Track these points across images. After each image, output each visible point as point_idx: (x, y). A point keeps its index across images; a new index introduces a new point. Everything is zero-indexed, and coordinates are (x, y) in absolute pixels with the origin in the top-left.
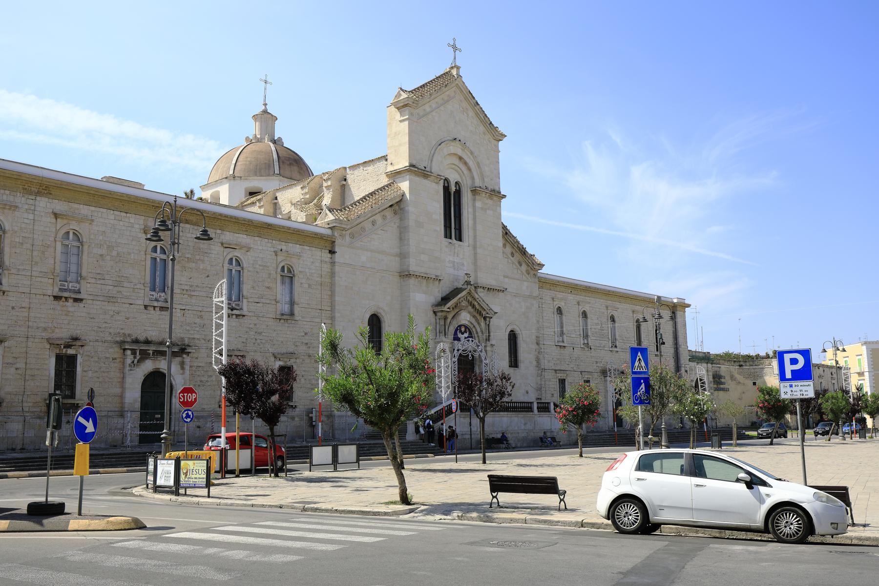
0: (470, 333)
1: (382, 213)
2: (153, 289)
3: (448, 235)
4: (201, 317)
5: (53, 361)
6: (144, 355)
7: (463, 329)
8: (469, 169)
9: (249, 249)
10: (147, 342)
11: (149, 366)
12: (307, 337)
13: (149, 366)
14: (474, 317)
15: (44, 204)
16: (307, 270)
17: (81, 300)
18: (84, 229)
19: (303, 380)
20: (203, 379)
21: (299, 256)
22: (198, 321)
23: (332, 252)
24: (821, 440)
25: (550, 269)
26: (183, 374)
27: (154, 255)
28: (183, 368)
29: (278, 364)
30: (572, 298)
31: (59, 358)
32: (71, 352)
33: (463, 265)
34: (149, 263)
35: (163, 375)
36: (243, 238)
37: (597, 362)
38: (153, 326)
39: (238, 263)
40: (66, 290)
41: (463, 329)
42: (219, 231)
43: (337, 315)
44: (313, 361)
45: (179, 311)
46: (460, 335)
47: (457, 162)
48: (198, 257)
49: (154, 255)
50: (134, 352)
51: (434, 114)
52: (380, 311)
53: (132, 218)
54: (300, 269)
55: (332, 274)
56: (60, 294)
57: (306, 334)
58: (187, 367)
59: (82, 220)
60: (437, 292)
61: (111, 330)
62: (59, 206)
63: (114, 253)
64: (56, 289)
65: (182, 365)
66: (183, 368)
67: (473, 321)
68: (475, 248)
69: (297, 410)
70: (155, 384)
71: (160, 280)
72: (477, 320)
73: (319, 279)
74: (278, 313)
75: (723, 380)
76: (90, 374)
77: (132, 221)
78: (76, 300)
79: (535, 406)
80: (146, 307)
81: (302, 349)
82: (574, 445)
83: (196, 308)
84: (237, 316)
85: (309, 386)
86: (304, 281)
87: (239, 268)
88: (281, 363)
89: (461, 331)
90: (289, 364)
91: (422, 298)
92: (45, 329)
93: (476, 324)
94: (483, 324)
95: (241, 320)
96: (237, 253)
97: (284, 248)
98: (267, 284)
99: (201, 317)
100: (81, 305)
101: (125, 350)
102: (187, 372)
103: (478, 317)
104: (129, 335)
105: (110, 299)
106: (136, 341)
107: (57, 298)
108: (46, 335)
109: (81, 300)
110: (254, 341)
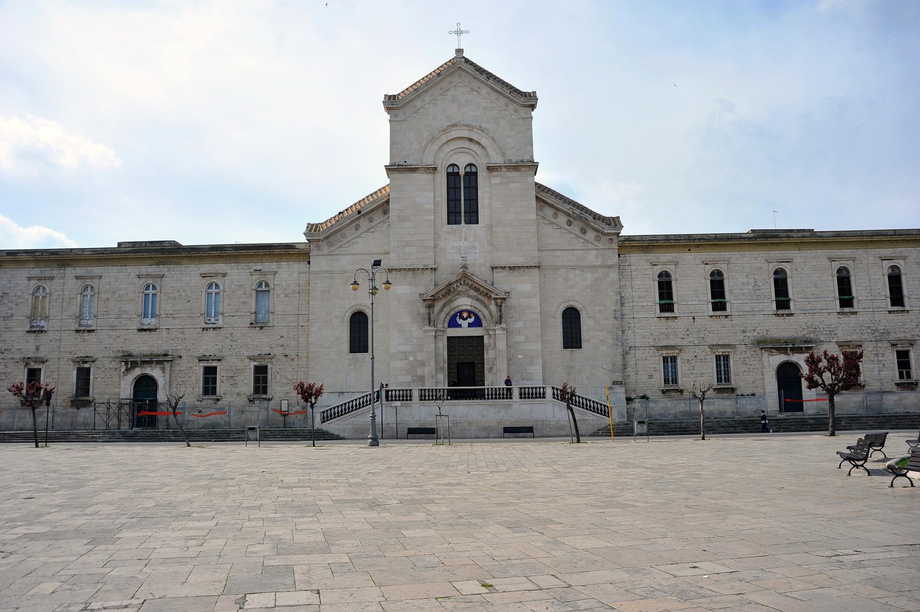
0: (455, 316)
1: (368, 217)
3: (453, 217)
4: (183, 333)
5: (75, 372)
6: (135, 364)
7: (465, 315)
9: (224, 275)
11: (137, 372)
13: (137, 372)
14: (478, 300)
15: (70, 272)
16: (284, 282)
17: (93, 331)
19: (278, 377)
23: (309, 263)
24: (725, 412)
29: (253, 364)
30: (863, 254)
31: (79, 370)
32: (86, 366)
33: (475, 247)
36: (220, 267)
37: (744, 332)
38: (142, 345)
39: (154, 287)
41: (465, 315)
46: (460, 321)
50: (126, 363)
56: (206, 326)
59: (92, 278)
60: (426, 285)
62: (80, 271)
63: (117, 295)
64: (28, 326)
67: (478, 305)
70: (145, 386)
72: (482, 303)
76: (99, 380)
82: (697, 432)
83: (178, 327)
84: (214, 329)
85: (285, 381)
86: (280, 292)
88: (256, 363)
90: (264, 363)
91: (406, 291)
92: (70, 353)
93: (481, 307)
95: (218, 331)
96: (214, 280)
98: (242, 300)
99: (183, 333)
100: (93, 334)
103: (486, 300)
105: (113, 328)
107: (77, 331)
108: (70, 356)
109: (93, 331)
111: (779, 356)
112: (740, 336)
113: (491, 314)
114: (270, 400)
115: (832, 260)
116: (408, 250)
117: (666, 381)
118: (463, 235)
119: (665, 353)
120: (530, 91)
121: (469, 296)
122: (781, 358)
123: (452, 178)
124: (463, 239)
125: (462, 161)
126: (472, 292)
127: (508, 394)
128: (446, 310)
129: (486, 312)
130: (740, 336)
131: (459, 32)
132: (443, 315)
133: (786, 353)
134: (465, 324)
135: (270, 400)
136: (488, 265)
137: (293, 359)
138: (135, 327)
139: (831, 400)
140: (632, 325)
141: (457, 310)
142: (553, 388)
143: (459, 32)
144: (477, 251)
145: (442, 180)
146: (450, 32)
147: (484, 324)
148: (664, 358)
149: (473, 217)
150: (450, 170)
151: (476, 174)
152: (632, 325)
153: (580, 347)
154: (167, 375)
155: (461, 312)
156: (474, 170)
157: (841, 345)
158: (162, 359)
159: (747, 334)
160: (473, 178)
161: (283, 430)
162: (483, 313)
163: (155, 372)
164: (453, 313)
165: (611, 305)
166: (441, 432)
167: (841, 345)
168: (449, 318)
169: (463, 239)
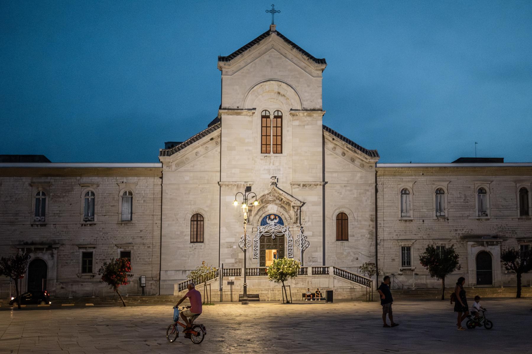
0: (265, 218)
1: (205, 146)
2: (37, 214)
3: (265, 149)
7: (272, 217)
10: (33, 244)
14: (282, 207)
16: (143, 192)
18: (133, 188)
20: (68, 261)
21: (136, 184)
22: (65, 230)
26: (53, 259)
27: (38, 197)
28: (52, 256)
29: (119, 250)
34: (34, 202)
35: (430, 250)
39: (93, 194)
40: (404, 216)
42: (79, 178)
44: (146, 247)
45: (52, 225)
46: (268, 221)
48: (64, 194)
49: (38, 197)
53: (24, 179)
57: (141, 231)
58: (55, 256)
61: (12, 239)
63: (14, 199)
65: (52, 255)
66: (52, 256)
67: (282, 210)
71: (40, 209)
72: (284, 208)
73: (153, 196)
74: (120, 220)
75: (430, 246)
77: (24, 180)
78: (41, 225)
80: (32, 225)
84: (90, 225)
87: (93, 197)
88: (122, 250)
89: (269, 218)
97: (125, 180)
101: (19, 249)
102: (55, 259)
103: (287, 207)
104: (23, 241)
106: (26, 244)
110: (102, 238)
111: (478, 247)
112: (453, 233)
113: (290, 217)
114: (132, 276)
115: (516, 182)
116: (233, 171)
117: (403, 264)
118: (272, 161)
119: (403, 244)
120: (322, 58)
121: (276, 204)
122: (480, 248)
123: (264, 119)
124: (271, 164)
125: (272, 108)
126: (278, 202)
127: (303, 272)
128: (260, 213)
129: (287, 216)
130: (453, 233)
131: (273, 12)
132: (258, 217)
133: (483, 245)
134: (272, 223)
135: (132, 276)
136: (289, 182)
137: (149, 247)
138: (29, 223)
139: (519, 277)
140: (382, 225)
141: (267, 213)
142: (334, 268)
143: (273, 12)
144: (281, 172)
145: (257, 119)
146: (267, 11)
147: (286, 223)
148: (402, 247)
149: (279, 149)
150: (264, 114)
151: (281, 117)
152: (382, 225)
153: (347, 240)
154: (55, 259)
155: (270, 215)
156: (280, 114)
157: (519, 240)
158: (50, 246)
159: (459, 232)
160: (279, 120)
161: (211, 304)
162: (285, 216)
163: (45, 256)
164: (264, 215)
165: (369, 212)
166: (261, 298)
167: (519, 240)
168: (260, 220)
169: (271, 164)
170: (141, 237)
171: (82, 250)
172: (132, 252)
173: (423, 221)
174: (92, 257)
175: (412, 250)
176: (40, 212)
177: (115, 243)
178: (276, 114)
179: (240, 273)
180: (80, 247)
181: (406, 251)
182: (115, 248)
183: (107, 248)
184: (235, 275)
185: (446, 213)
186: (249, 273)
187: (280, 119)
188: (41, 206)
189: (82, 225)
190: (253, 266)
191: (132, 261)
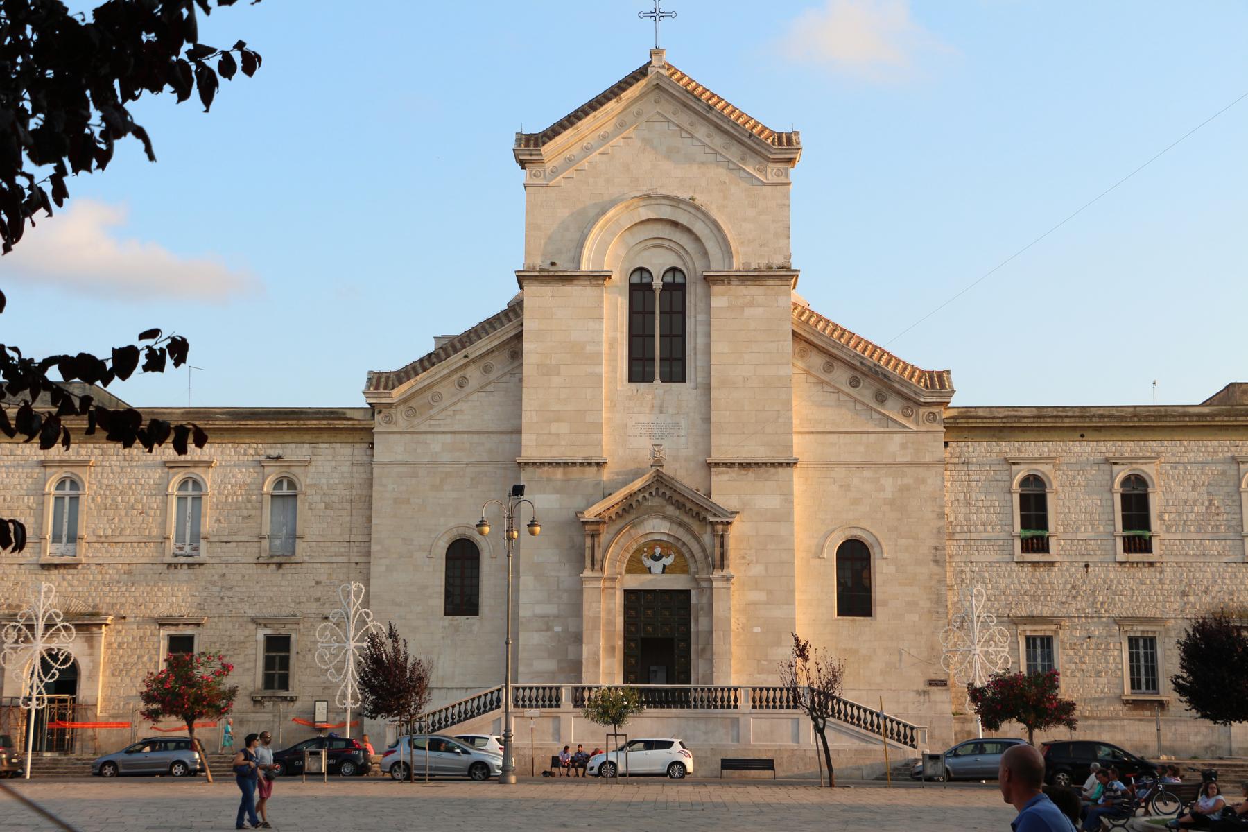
3: (639, 370)
8: (697, 239)
12: (320, 588)
13: (40, 645)
14: (681, 524)
25: (967, 394)
43: (375, 547)
47: (667, 232)
49: (60, 493)
51: (595, 156)
52: (860, 534)
54: (309, 481)
55: (370, 482)
56: (175, 560)
57: (318, 583)
67: (680, 533)
68: (708, 388)
69: (298, 704)
72: (688, 529)
73: (348, 493)
79: (744, 703)
81: (311, 608)
84: (190, 565)
86: (317, 498)
88: (269, 632)
90: (283, 632)
93: (686, 538)
94: (707, 538)
95: (199, 570)
98: (245, 513)
114: (292, 700)
116: (554, 428)
131: (657, 15)
143: (657, 15)
144: (683, 432)
150: (636, 279)
156: (679, 279)
160: (677, 295)
170: (318, 599)
171: (164, 633)
172: (293, 638)
173: (1087, 566)
174: (288, 650)
175: (1056, 645)
176: (65, 532)
177: (251, 613)
178: (669, 279)
179: (558, 699)
180: (162, 623)
181: (1143, 651)
182: (252, 627)
183: (230, 626)
184: (537, 706)
185: (885, 555)
186: (722, 701)
187: (679, 293)
188: (66, 519)
189: (169, 565)
190: (604, 683)
191: (292, 661)
